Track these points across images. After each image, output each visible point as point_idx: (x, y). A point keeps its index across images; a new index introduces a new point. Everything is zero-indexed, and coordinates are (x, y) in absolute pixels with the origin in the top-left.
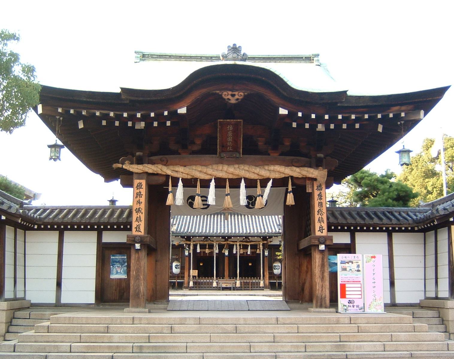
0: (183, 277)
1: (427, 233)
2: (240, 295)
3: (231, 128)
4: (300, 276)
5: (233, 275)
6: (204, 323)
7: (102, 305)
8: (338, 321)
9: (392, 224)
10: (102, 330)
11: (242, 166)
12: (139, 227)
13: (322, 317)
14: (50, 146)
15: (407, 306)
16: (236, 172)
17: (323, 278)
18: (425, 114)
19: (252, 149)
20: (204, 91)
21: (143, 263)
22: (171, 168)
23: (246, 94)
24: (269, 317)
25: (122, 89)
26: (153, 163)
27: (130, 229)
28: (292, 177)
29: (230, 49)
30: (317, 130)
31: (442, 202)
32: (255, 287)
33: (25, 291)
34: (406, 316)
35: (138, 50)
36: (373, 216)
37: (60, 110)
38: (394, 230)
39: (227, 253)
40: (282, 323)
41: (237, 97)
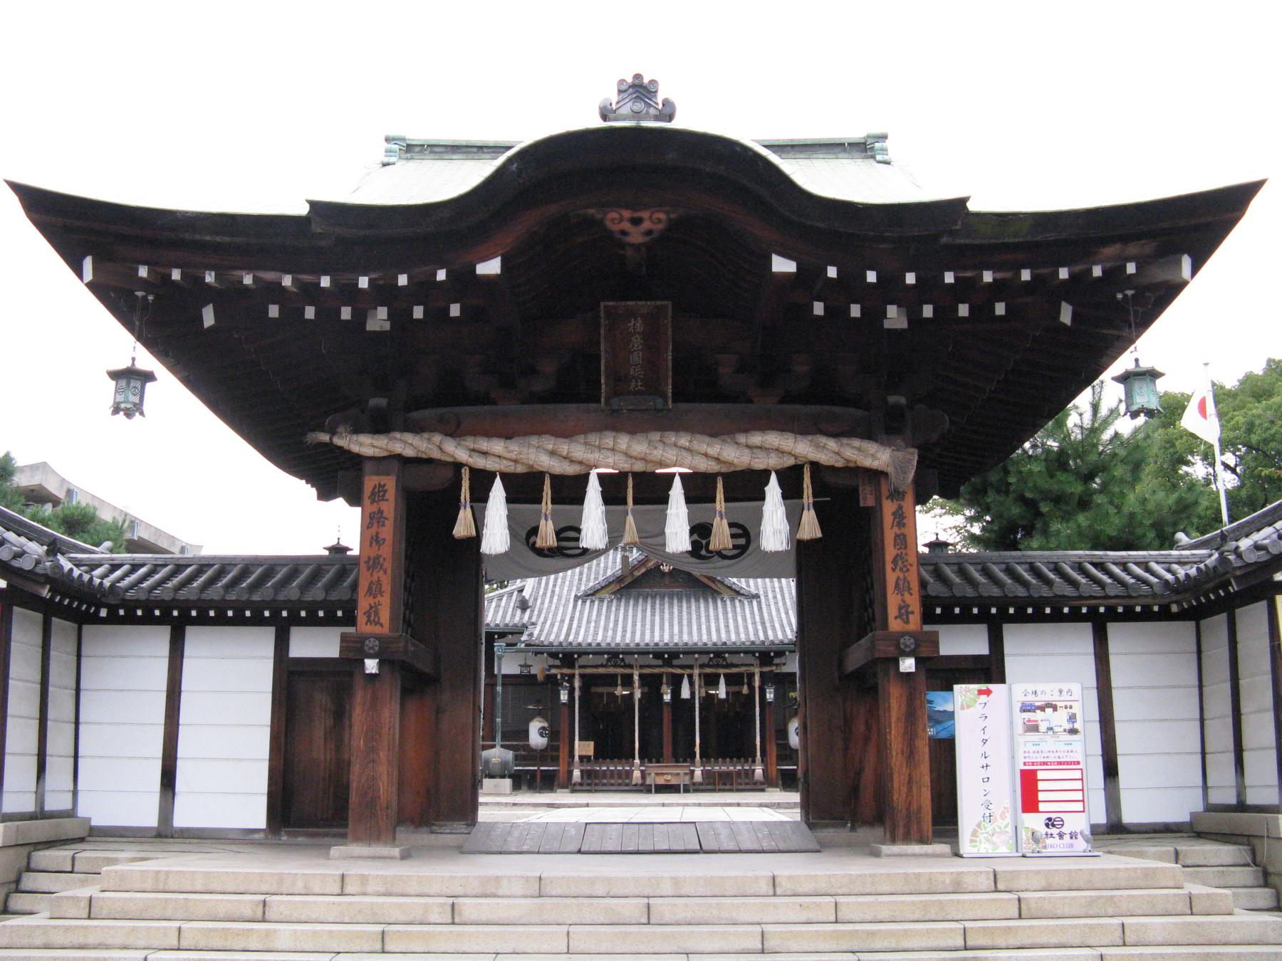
0: (555, 760)
1: (1203, 623)
2: (700, 805)
3: (640, 326)
4: (846, 748)
5: (683, 754)
6: (554, 893)
7: (288, 834)
8: (958, 884)
9: (1107, 597)
10: (248, 913)
11: (672, 437)
12: (379, 611)
13: (909, 871)
14: (115, 375)
15: (1155, 832)
16: (655, 452)
17: (911, 754)
18: (1195, 269)
19: (699, 390)
20: (553, 209)
21: (394, 716)
22: (470, 442)
23: (673, 216)
24: (750, 874)
25: (313, 204)
26: (417, 429)
27: (350, 620)
28: (815, 466)
29: (623, 88)
30: (887, 324)
31: (1246, 530)
32: (745, 783)
33: (75, 793)
34: (1150, 860)
35: (392, 134)
36: (1052, 576)
37: (143, 272)
38: (1113, 616)
39: (667, 698)
40: (789, 892)
41: (647, 225)
